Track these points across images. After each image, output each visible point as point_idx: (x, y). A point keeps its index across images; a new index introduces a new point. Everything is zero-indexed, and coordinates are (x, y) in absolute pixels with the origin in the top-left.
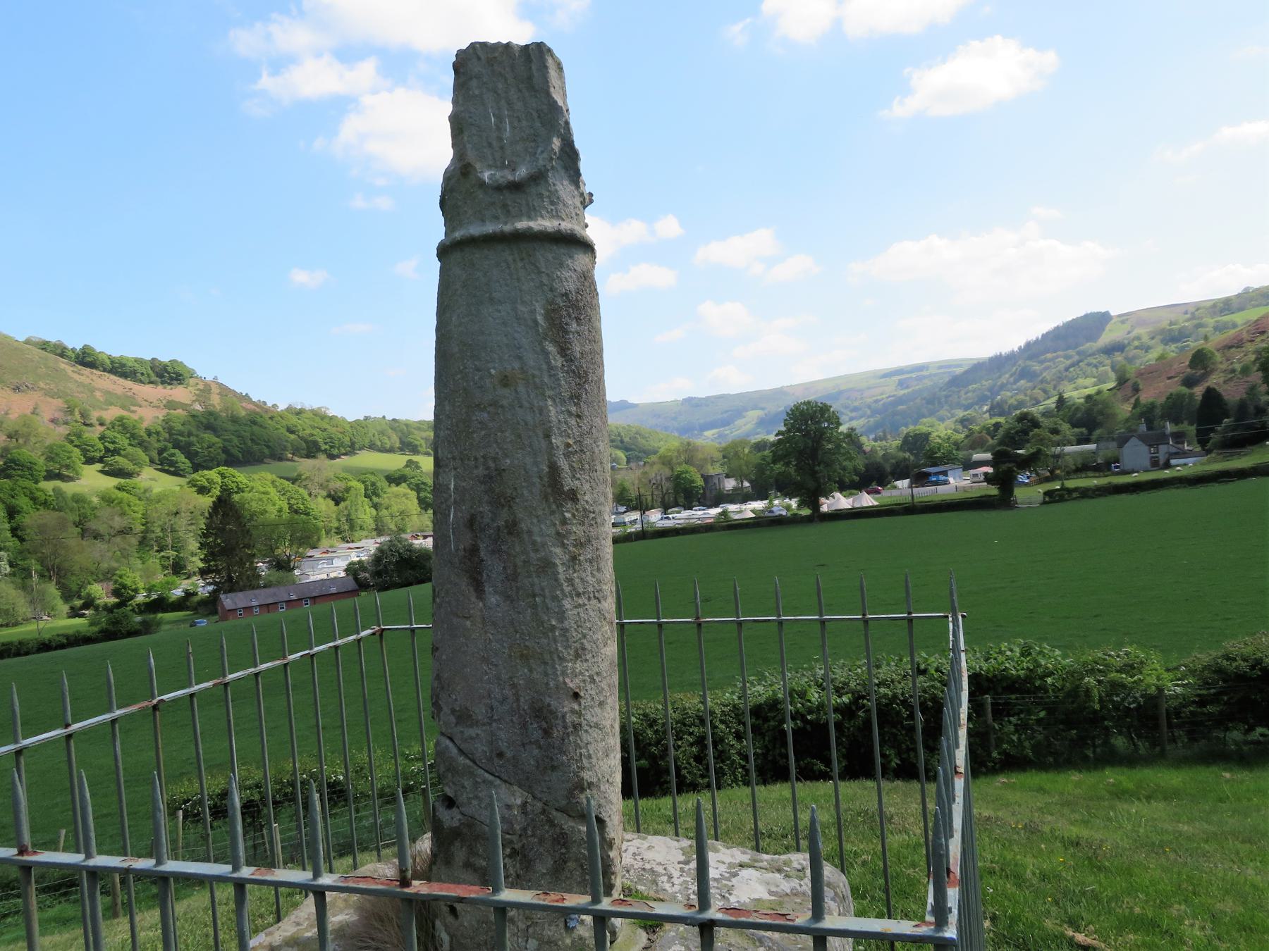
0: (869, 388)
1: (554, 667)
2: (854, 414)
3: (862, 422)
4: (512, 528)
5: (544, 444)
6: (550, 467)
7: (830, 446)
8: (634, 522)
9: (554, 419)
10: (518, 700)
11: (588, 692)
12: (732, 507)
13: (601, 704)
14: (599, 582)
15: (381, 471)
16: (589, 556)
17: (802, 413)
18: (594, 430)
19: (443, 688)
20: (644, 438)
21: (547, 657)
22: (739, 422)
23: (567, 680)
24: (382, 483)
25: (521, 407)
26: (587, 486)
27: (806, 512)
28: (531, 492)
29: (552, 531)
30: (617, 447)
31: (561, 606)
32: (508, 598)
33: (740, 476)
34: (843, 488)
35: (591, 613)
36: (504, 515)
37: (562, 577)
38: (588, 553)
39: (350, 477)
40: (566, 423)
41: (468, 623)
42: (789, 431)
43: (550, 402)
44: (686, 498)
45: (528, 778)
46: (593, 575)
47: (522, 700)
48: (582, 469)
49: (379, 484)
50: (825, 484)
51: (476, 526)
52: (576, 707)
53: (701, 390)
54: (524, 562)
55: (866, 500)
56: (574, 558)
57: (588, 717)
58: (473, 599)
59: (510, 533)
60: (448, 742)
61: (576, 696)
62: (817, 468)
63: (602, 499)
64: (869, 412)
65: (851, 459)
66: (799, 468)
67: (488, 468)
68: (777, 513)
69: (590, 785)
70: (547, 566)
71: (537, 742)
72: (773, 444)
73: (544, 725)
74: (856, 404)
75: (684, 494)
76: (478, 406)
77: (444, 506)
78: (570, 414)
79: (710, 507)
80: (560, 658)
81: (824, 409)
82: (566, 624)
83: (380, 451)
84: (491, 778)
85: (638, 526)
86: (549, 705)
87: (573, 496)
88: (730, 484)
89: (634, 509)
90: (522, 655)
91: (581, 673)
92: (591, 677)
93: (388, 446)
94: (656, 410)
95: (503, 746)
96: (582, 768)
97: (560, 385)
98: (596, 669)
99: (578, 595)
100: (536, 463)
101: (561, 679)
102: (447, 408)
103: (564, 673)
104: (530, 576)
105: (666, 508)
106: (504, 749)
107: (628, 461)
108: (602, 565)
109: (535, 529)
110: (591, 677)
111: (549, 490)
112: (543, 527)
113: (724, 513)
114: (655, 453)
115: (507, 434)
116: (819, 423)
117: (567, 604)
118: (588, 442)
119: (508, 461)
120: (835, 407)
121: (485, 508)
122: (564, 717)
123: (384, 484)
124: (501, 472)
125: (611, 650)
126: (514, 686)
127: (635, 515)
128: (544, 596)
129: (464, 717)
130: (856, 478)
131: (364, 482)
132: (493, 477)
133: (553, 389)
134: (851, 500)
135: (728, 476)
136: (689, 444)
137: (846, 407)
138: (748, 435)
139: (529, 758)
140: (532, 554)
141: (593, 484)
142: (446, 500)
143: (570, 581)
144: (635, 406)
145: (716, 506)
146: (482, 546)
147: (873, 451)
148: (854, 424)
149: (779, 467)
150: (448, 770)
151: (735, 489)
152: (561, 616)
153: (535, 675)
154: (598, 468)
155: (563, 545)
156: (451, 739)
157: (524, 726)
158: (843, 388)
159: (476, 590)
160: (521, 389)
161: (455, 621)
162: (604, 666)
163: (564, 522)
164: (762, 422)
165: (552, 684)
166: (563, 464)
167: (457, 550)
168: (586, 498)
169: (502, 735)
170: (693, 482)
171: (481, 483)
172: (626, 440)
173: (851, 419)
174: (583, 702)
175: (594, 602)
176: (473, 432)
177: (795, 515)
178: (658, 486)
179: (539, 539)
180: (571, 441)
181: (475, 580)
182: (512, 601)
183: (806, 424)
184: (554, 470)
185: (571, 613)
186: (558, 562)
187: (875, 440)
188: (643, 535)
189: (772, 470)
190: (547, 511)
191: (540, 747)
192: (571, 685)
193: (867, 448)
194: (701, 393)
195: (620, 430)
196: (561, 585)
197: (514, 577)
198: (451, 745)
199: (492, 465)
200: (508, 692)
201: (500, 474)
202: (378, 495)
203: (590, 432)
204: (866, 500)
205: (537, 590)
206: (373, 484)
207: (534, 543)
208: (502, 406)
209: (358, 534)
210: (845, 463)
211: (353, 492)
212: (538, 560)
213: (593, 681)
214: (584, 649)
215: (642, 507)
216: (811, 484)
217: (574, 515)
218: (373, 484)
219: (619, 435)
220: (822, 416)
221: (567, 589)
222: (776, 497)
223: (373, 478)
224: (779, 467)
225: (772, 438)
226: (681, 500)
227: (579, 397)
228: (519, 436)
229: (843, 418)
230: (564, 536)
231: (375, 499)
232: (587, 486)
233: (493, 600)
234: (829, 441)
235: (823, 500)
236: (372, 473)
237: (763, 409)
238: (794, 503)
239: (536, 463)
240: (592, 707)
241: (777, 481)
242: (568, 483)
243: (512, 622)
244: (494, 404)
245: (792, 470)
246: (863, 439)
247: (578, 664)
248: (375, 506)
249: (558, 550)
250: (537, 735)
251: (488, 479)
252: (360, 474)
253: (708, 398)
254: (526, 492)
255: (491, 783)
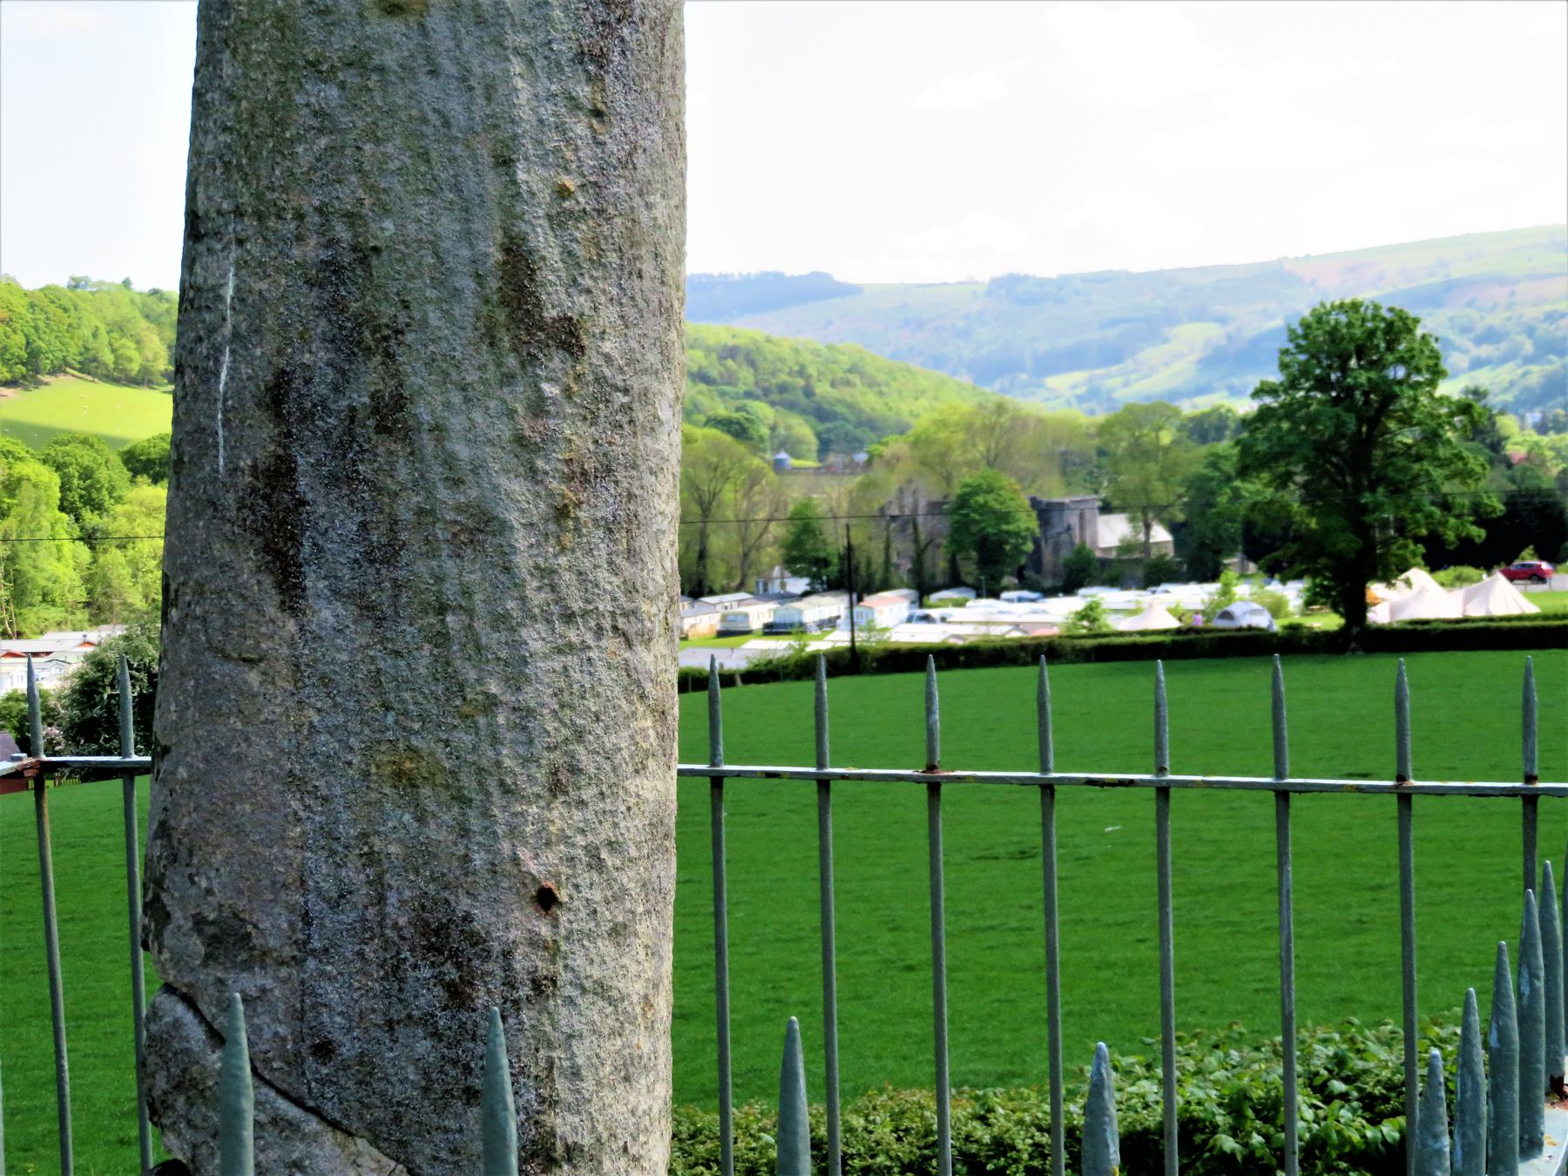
0: (1533, 277)
1: (486, 814)
2: (1485, 351)
3: (1507, 373)
4: (390, 414)
5: (493, 184)
6: (507, 251)
7: (1407, 437)
8: (831, 623)
9: (525, 113)
10: (381, 899)
11: (581, 894)
12: (1110, 597)
13: (618, 932)
14: (631, 590)
15: (112, 441)
16: (604, 512)
17: (1333, 334)
18: (640, 159)
19: (174, 859)
20: (872, 383)
21: (468, 782)
22: (1150, 354)
23: (524, 854)
24: (113, 473)
25: (433, 73)
26: (609, 314)
27: (1328, 621)
28: (447, 314)
29: (504, 430)
30: (792, 406)
31: (516, 644)
32: (368, 610)
33: (1143, 510)
34: (1437, 559)
35: (603, 673)
36: (370, 380)
37: (523, 563)
38: (595, 506)
39: (20, 450)
40: (561, 128)
41: (253, 677)
42: (1293, 384)
43: (517, 66)
44: (983, 563)
45: (397, 1119)
46: (614, 568)
47: (392, 898)
48: (598, 263)
49: (102, 475)
50: (1386, 543)
51: (289, 407)
52: (545, 931)
53: (1047, 259)
54: (421, 512)
55: (1501, 597)
56: (561, 513)
57: (579, 961)
58: (272, 611)
59: (382, 429)
60: (180, 1009)
61: (546, 900)
62: (1366, 498)
63: (653, 358)
64: (1528, 347)
65: (1465, 475)
66: (1311, 494)
67: (332, 243)
68: (1245, 622)
69: (572, 1152)
70: (482, 527)
71: (427, 1020)
72: (1245, 423)
73: (453, 974)
74: (1496, 320)
75: (982, 553)
76: (314, 64)
77: (203, 349)
78: (573, 103)
79: (1049, 593)
80: (506, 790)
81: (1396, 328)
82: (528, 696)
83: (116, 381)
84: (293, 1112)
85: (839, 639)
86: (468, 918)
87: (569, 337)
88: (1112, 532)
89: (833, 586)
90: (399, 774)
91: (565, 839)
92: (593, 852)
93: (135, 367)
94: (913, 312)
95: (333, 1024)
96: (553, 1103)
97: (548, 19)
98: (606, 831)
99: (569, 617)
100: (468, 236)
101: (505, 847)
102: (227, 70)
103: (514, 832)
104: (433, 554)
105: (923, 588)
106: (337, 1036)
107: (825, 446)
108: (641, 542)
109: (456, 423)
110: (593, 852)
111: (501, 315)
112: (478, 416)
113: (1088, 614)
114: (902, 430)
115: (390, 148)
116: (1378, 365)
117: (535, 639)
118: (619, 188)
119: (389, 225)
120: (1430, 323)
121: (317, 356)
122: (507, 954)
123: (120, 474)
124: (365, 255)
125: (658, 787)
126: (370, 858)
127: (833, 605)
128: (470, 612)
129: (228, 940)
130: (1478, 533)
131: (59, 467)
132: (344, 269)
133: (527, 30)
134: (1458, 594)
135: (1106, 509)
136: (1000, 409)
137: (1465, 330)
138: (1176, 394)
139: (408, 1060)
140: (443, 493)
141: (631, 313)
142: (212, 330)
143: (547, 574)
144: (849, 290)
145: (1069, 589)
146: (302, 462)
147: (1534, 458)
148: (1483, 378)
149: (1256, 488)
150: (178, 1087)
151: (1126, 548)
152: (517, 670)
153: (432, 831)
154: (648, 267)
155: (533, 473)
156: (190, 1002)
157: (395, 971)
158: (1456, 272)
159: (279, 585)
160: (437, 22)
161: (220, 670)
162: (633, 829)
163: (539, 407)
164: (1217, 361)
165: (479, 859)
166: (545, 243)
167: (234, 470)
168: (607, 347)
169: (331, 993)
170: (1005, 517)
171: (309, 283)
172: (822, 389)
173: (1477, 364)
174: (564, 917)
175: (611, 642)
176: (298, 139)
177: (1295, 628)
178: (908, 523)
179: (463, 451)
180: (571, 182)
181: (279, 555)
182: (380, 621)
183: (1344, 369)
184: (518, 260)
185: (545, 668)
186: (513, 517)
187: (1542, 429)
188: (849, 663)
189: (1237, 495)
190: (491, 374)
191: (436, 1035)
192: (533, 867)
193: (1515, 449)
194: (1046, 265)
195: (807, 358)
196: (520, 586)
197: (390, 553)
198: (188, 1017)
199: (342, 232)
200: (354, 875)
201: (364, 261)
202: (98, 507)
203: (628, 163)
204: (1501, 597)
205: (450, 591)
206: (87, 474)
207: (450, 461)
208: (381, 69)
209: (35, 614)
210: (1446, 488)
211: (26, 491)
212: (459, 509)
213: (597, 864)
214: (575, 770)
215: (851, 579)
216: (1346, 542)
217: (567, 392)
218: (87, 474)
219: (802, 372)
220: (1391, 347)
221: (537, 598)
222: (1244, 576)
223: (85, 457)
224: (1256, 488)
225: (1246, 407)
226: (969, 569)
227: (601, 59)
228: (425, 157)
229: (1451, 361)
230: (537, 449)
231: (91, 518)
232: (609, 314)
233: (325, 614)
234: (1406, 420)
235: (1376, 589)
236: (85, 442)
237: (1222, 320)
238: (1292, 593)
239: (468, 236)
240: (589, 935)
241: (1249, 526)
242: (555, 300)
243: (376, 678)
244: (359, 62)
245: (1292, 498)
246: (1507, 424)
247: (558, 811)
248: (90, 538)
249: (518, 487)
250: (429, 998)
251: (330, 273)
252: (54, 447)
253: (1065, 280)
254: (434, 318)
255: (293, 1126)
